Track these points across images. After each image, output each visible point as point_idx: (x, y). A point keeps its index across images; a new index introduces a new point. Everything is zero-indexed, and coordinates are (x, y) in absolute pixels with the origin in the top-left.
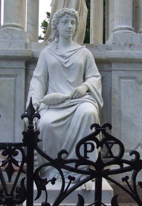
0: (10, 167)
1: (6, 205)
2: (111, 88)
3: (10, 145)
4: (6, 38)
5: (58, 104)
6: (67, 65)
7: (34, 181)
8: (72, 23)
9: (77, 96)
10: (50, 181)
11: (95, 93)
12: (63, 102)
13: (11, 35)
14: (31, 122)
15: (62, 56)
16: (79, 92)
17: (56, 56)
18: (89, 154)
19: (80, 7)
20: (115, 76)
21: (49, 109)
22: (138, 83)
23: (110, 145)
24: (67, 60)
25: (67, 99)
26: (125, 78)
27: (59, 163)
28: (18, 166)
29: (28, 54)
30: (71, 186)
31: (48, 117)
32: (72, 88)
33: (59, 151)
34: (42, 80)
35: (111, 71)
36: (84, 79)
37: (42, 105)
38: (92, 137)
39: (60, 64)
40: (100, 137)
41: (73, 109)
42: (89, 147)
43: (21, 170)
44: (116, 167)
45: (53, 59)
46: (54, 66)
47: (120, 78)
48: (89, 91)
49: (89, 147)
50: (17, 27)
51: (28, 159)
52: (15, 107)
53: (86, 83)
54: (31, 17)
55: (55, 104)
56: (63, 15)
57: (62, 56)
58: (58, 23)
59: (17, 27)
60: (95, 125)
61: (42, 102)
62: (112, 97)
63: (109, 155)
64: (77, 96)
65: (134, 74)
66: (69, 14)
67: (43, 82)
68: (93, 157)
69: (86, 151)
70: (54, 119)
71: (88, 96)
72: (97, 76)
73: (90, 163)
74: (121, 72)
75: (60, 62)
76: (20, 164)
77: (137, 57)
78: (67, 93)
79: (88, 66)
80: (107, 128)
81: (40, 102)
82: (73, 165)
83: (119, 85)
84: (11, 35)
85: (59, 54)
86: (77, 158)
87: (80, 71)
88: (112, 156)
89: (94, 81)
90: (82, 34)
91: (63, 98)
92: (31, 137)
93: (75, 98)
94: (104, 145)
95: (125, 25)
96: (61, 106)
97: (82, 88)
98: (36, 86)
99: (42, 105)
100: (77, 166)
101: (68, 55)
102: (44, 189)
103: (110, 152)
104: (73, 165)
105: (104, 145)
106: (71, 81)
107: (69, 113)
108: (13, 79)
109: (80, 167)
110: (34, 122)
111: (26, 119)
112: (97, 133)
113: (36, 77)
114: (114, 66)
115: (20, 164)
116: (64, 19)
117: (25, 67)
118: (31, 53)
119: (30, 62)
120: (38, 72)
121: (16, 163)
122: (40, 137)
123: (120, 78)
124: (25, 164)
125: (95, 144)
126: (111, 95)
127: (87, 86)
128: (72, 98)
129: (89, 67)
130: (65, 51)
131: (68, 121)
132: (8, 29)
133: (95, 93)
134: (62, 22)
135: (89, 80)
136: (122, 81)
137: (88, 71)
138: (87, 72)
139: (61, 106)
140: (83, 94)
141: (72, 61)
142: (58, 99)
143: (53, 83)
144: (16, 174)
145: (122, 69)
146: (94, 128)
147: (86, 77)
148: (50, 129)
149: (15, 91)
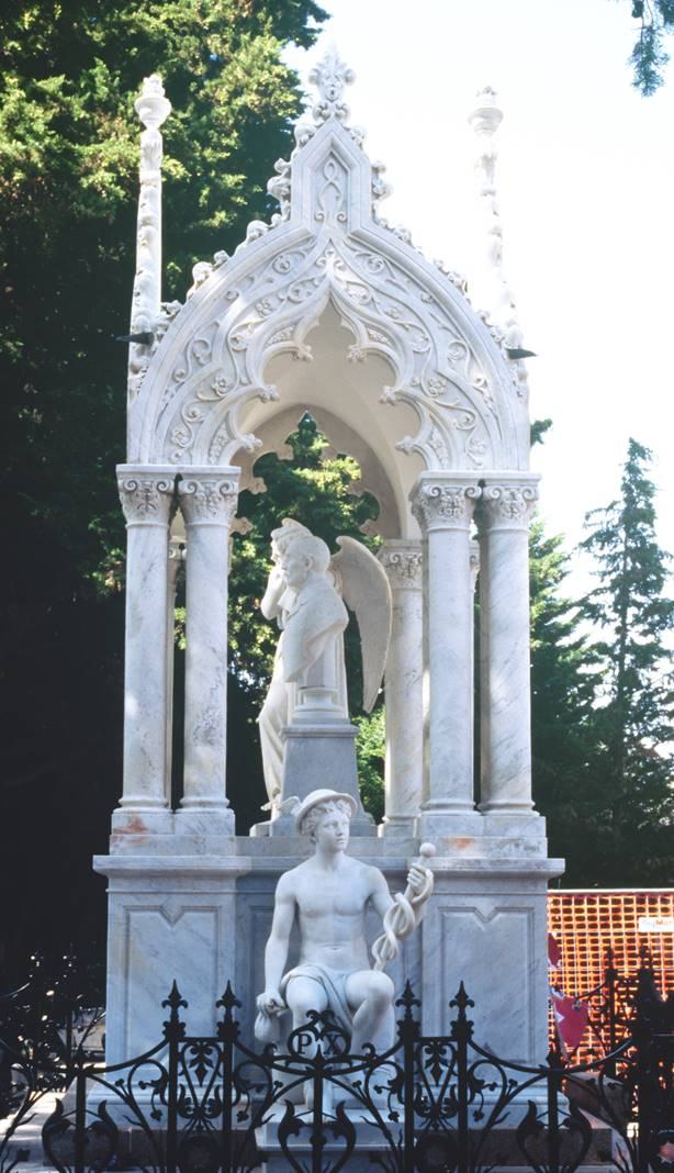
3: (202, 1040)
7: (76, 1079)
10: (488, 1085)
14: (408, 1010)
18: (304, 1049)
23: (333, 1038)
28: (212, 1066)
30: (513, 1090)
38: (310, 1027)
42: (305, 1040)
43: (451, 1072)
49: (305, 1040)
51: (460, 1057)
60: (311, 1013)
69: (300, 1045)
77: (129, 866)
82: (281, 1063)
86: (289, 1055)
100: (287, 1064)
104: (281, 1063)
109: (293, 1066)
111: (456, 1008)
115: (215, 1065)
121: (210, 1063)
122: (473, 1028)
123: (128, 909)
136: (133, 915)
144: (443, 1077)
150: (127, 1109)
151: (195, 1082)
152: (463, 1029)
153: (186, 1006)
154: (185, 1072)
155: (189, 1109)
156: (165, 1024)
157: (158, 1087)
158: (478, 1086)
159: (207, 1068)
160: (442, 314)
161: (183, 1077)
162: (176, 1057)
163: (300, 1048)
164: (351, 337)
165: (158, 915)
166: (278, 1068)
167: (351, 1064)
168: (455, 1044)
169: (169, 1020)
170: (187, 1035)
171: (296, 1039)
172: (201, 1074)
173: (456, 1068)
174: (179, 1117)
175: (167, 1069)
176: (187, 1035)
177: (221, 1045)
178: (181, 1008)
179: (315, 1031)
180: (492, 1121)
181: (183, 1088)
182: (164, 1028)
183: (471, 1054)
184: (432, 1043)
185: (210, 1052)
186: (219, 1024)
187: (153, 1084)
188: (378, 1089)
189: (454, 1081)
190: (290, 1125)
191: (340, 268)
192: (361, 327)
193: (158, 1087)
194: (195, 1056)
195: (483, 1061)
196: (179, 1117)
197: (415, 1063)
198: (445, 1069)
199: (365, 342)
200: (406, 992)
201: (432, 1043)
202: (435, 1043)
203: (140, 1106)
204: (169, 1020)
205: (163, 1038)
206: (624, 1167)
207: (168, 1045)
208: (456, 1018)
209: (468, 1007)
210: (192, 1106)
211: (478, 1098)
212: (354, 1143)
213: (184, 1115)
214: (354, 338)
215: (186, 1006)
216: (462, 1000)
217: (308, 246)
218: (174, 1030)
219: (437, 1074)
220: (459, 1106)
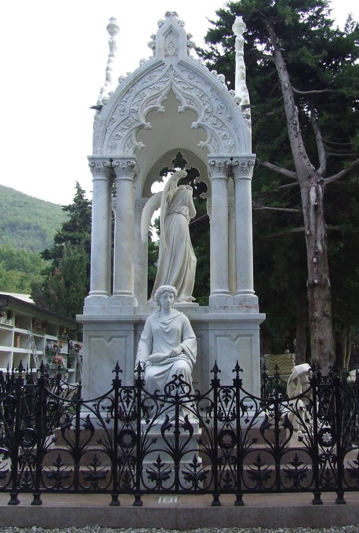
0: (128, 399)
1: (246, 42)
2: (208, 345)
4: (117, 304)
5: (160, 362)
6: (167, 331)
8: (171, 297)
9: (174, 355)
11: (189, 353)
12: (163, 360)
13: (122, 302)
15: (163, 323)
16: (175, 353)
17: (158, 323)
19: (187, 261)
20: (211, 335)
21: (152, 365)
22: (232, 340)
24: (167, 327)
25: (167, 357)
26: (220, 336)
27: (155, 397)
29: (138, 319)
31: (152, 372)
32: (171, 348)
33: (155, 390)
34: (148, 342)
35: (208, 330)
36: (182, 341)
37: (148, 363)
38: (173, 382)
39: (161, 329)
40: (177, 382)
41: (170, 365)
44: (186, 399)
45: (156, 326)
46: (157, 331)
47: (216, 336)
48: (183, 351)
50: (126, 293)
51: (237, 394)
52: (125, 364)
53: (182, 345)
54: (139, 255)
55: (156, 362)
56: (164, 292)
57: (163, 323)
58: (160, 297)
59: (126, 293)
61: (147, 360)
62: (210, 353)
63: (182, 392)
64: (174, 355)
65: (228, 333)
66: (168, 291)
67: (149, 344)
68: (173, 393)
69: (170, 390)
70: (156, 373)
71: (182, 355)
72: (191, 338)
73: (172, 397)
74: (217, 331)
75: (161, 327)
76: (133, 398)
77: (229, 318)
78: (167, 353)
79: (184, 330)
80: (182, 377)
81: (146, 360)
83: (216, 342)
84: (122, 302)
85: (161, 321)
87: (178, 334)
88: (184, 393)
89: (190, 343)
90: (191, 285)
91: (163, 357)
92: (139, 383)
93: (173, 357)
94: (180, 386)
95: (220, 289)
96: (162, 363)
97: (178, 349)
98: (143, 347)
99: (148, 363)
101: (167, 322)
102: (147, 412)
103: (183, 390)
105: (180, 386)
106: (170, 343)
107: (168, 368)
108: (124, 339)
110: (141, 376)
112: (176, 379)
113: (144, 340)
114: (210, 327)
115: (133, 398)
116: (164, 295)
117: (134, 329)
118: (139, 318)
119: (138, 325)
120: (144, 336)
121: (131, 397)
124: (136, 398)
125: (175, 386)
126: (208, 351)
127: (182, 347)
128: (170, 357)
129: (185, 331)
130: (166, 319)
131: (165, 376)
132: (119, 296)
133: (189, 353)
134: (163, 297)
135: (184, 342)
136: (218, 338)
137: (185, 334)
138: (185, 334)
139: (162, 363)
140: (179, 353)
141: (171, 326)
142: (159, 358)
143: (156, 344)
145: (218, 328)
146: (174, 377)
147: (184, 338)
148: (153, 380)
149: (125, 350)
150: (98, 420)
151: (224, 406)
152: (238, 383)
153: (220, 372)
154: (220, 401)
155: (223, 417)
156: (113, 380)
157: (110, 409)
158: (245, 409)
159: (130, 399)
160: (141, 80)
161: (220, 403)
162: (216, 395)
163: (170, 392)
164: (179, 102)
165: (240, 338)
166: (161, 400)
167: (190, 398)
168: (235, 389)
169: (235, 378)
170: (221, 385)
171: (168, 387)
172: (128, 402)
173: (235, 399)
174: (218, 421)
175: (213, 401)
176: (221, 385)
177: (235, 389)
178: (240, 372)
179: (176, 384)
180: (251, 425)
181: (220, 407)
182: (112, 382)
183: (242, 395)
184: (225, 388)
185: (131, 392)
186: (135, 380)
187: (108, 408)
188: (103, 408)
189: (234, 404)
190: (166, 427)
191: (176, 77)
192: (183, 98)
193: (110, 409)
194: (224, 394)
195: (148, 398)
196: (218, 421)
197: (218, 397)
198: (132, 401)
199: (185, 103)
200: (236, 366)
201: (225, 388)
202: (227, 389)
203: (91, 420)
204: (235, 378)
205: (112, 387)
206: (308, 445)
207: (114, 391)
208: (213, 378)
209: (219, 372)
210: (224, 415)
211: (246, 415)
212: (193, 433)
213: (221, 420)
214: (181, 103)
215: (220, 372)
216: (237, 369)
217: (163, 67)
218: (117, 383)
219: (128, 402)
220: (236, 416)
